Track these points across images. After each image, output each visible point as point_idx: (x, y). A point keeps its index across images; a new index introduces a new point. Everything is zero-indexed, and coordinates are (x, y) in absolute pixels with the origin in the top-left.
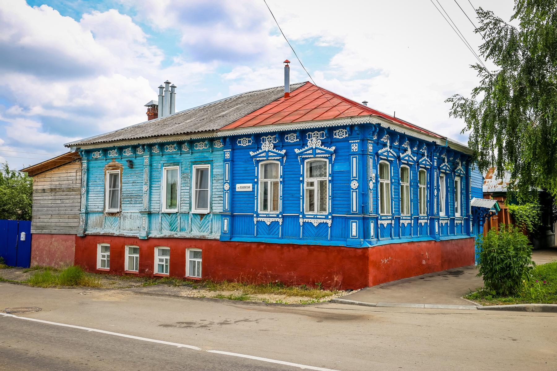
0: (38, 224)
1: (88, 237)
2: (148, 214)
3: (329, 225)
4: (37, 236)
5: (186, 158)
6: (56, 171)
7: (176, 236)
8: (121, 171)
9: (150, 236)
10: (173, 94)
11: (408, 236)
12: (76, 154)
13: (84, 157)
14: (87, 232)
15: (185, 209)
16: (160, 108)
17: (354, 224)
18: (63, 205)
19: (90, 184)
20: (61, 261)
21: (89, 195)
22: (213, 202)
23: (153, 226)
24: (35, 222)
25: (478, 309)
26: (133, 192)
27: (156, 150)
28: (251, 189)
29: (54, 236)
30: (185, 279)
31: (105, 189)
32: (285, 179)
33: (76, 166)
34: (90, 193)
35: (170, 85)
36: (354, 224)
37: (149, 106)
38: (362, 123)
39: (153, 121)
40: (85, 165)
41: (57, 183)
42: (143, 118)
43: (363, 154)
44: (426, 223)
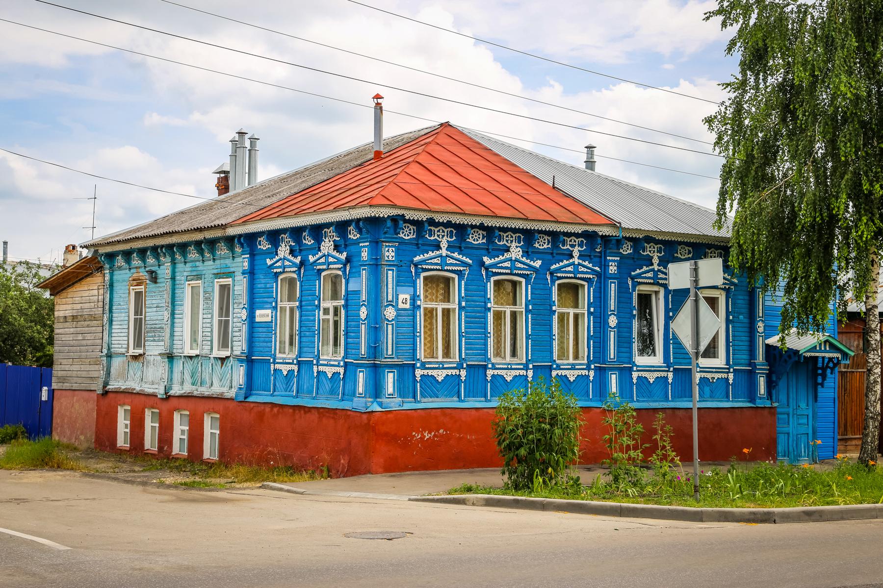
0: (60, 374)
1: (111, 395)
2: (168, 357)
3: (463, 378)
4: (59, 392)
5: (209, 267)
6: (77, 287)
7: (195, 393)
8: (146, 288)
9: (172, 393)
10: (253, 152)
11: (483, 399)
12: (94, 259)
13: (107, 266)
14: (109, 387)
15: (206, 351)
16: (231, 176)
17: (391, 375)
18: (84, 342)
19: (114, 308)
20: (82, 434)
21: (113, 327)
22: (235, 339)
23: (177, 376)
24: (58, 370)
25: (410, 500)
26: (157, 322)
27: (120, 261)
28: (269, 319)
29: (77, 392)
30: (203, 462)
31: (129, 317)
32: (303, 303)
33: (97, 279)
34: (114, 323)
35: (247, 136)
36: (614, 376)
37: (220, 173)
38: (381, 216)
39: (223, 197)
40: (107, 278)
41: (78, 306)
42: (212, 194)
43: (376, 265)
44: (291, 372)
